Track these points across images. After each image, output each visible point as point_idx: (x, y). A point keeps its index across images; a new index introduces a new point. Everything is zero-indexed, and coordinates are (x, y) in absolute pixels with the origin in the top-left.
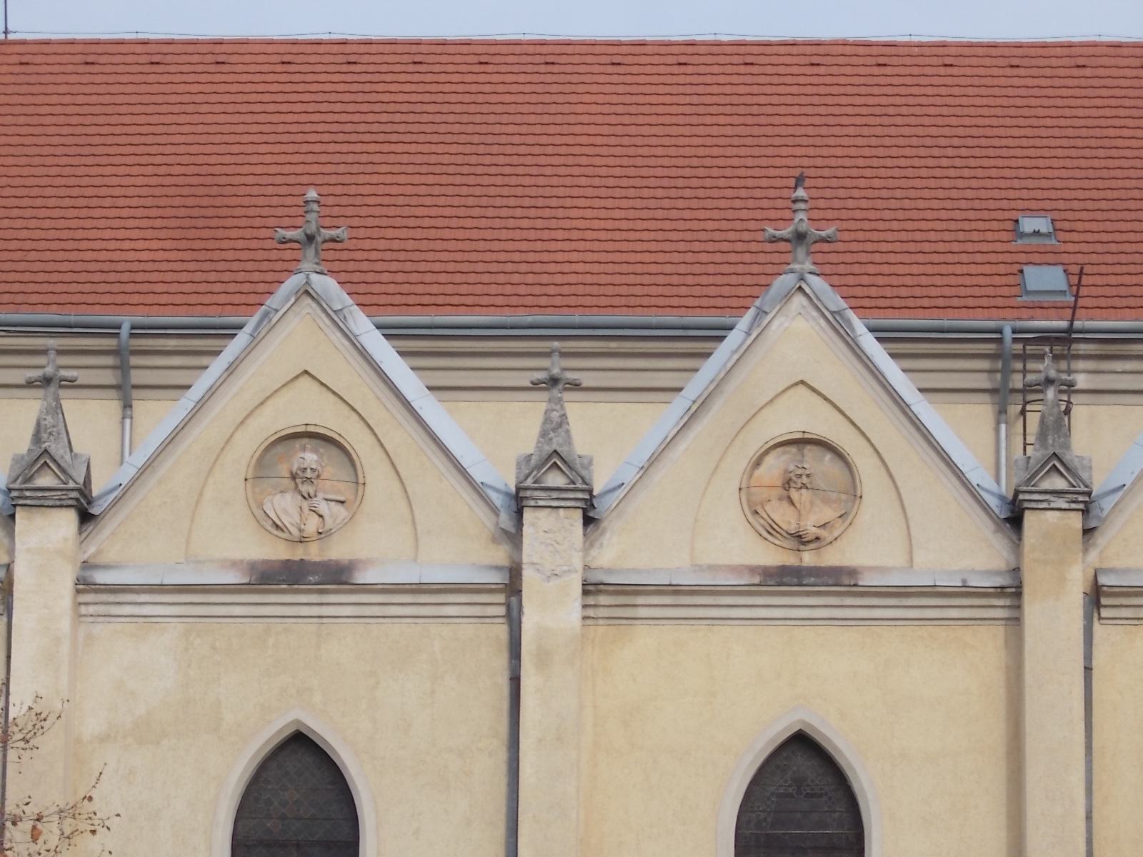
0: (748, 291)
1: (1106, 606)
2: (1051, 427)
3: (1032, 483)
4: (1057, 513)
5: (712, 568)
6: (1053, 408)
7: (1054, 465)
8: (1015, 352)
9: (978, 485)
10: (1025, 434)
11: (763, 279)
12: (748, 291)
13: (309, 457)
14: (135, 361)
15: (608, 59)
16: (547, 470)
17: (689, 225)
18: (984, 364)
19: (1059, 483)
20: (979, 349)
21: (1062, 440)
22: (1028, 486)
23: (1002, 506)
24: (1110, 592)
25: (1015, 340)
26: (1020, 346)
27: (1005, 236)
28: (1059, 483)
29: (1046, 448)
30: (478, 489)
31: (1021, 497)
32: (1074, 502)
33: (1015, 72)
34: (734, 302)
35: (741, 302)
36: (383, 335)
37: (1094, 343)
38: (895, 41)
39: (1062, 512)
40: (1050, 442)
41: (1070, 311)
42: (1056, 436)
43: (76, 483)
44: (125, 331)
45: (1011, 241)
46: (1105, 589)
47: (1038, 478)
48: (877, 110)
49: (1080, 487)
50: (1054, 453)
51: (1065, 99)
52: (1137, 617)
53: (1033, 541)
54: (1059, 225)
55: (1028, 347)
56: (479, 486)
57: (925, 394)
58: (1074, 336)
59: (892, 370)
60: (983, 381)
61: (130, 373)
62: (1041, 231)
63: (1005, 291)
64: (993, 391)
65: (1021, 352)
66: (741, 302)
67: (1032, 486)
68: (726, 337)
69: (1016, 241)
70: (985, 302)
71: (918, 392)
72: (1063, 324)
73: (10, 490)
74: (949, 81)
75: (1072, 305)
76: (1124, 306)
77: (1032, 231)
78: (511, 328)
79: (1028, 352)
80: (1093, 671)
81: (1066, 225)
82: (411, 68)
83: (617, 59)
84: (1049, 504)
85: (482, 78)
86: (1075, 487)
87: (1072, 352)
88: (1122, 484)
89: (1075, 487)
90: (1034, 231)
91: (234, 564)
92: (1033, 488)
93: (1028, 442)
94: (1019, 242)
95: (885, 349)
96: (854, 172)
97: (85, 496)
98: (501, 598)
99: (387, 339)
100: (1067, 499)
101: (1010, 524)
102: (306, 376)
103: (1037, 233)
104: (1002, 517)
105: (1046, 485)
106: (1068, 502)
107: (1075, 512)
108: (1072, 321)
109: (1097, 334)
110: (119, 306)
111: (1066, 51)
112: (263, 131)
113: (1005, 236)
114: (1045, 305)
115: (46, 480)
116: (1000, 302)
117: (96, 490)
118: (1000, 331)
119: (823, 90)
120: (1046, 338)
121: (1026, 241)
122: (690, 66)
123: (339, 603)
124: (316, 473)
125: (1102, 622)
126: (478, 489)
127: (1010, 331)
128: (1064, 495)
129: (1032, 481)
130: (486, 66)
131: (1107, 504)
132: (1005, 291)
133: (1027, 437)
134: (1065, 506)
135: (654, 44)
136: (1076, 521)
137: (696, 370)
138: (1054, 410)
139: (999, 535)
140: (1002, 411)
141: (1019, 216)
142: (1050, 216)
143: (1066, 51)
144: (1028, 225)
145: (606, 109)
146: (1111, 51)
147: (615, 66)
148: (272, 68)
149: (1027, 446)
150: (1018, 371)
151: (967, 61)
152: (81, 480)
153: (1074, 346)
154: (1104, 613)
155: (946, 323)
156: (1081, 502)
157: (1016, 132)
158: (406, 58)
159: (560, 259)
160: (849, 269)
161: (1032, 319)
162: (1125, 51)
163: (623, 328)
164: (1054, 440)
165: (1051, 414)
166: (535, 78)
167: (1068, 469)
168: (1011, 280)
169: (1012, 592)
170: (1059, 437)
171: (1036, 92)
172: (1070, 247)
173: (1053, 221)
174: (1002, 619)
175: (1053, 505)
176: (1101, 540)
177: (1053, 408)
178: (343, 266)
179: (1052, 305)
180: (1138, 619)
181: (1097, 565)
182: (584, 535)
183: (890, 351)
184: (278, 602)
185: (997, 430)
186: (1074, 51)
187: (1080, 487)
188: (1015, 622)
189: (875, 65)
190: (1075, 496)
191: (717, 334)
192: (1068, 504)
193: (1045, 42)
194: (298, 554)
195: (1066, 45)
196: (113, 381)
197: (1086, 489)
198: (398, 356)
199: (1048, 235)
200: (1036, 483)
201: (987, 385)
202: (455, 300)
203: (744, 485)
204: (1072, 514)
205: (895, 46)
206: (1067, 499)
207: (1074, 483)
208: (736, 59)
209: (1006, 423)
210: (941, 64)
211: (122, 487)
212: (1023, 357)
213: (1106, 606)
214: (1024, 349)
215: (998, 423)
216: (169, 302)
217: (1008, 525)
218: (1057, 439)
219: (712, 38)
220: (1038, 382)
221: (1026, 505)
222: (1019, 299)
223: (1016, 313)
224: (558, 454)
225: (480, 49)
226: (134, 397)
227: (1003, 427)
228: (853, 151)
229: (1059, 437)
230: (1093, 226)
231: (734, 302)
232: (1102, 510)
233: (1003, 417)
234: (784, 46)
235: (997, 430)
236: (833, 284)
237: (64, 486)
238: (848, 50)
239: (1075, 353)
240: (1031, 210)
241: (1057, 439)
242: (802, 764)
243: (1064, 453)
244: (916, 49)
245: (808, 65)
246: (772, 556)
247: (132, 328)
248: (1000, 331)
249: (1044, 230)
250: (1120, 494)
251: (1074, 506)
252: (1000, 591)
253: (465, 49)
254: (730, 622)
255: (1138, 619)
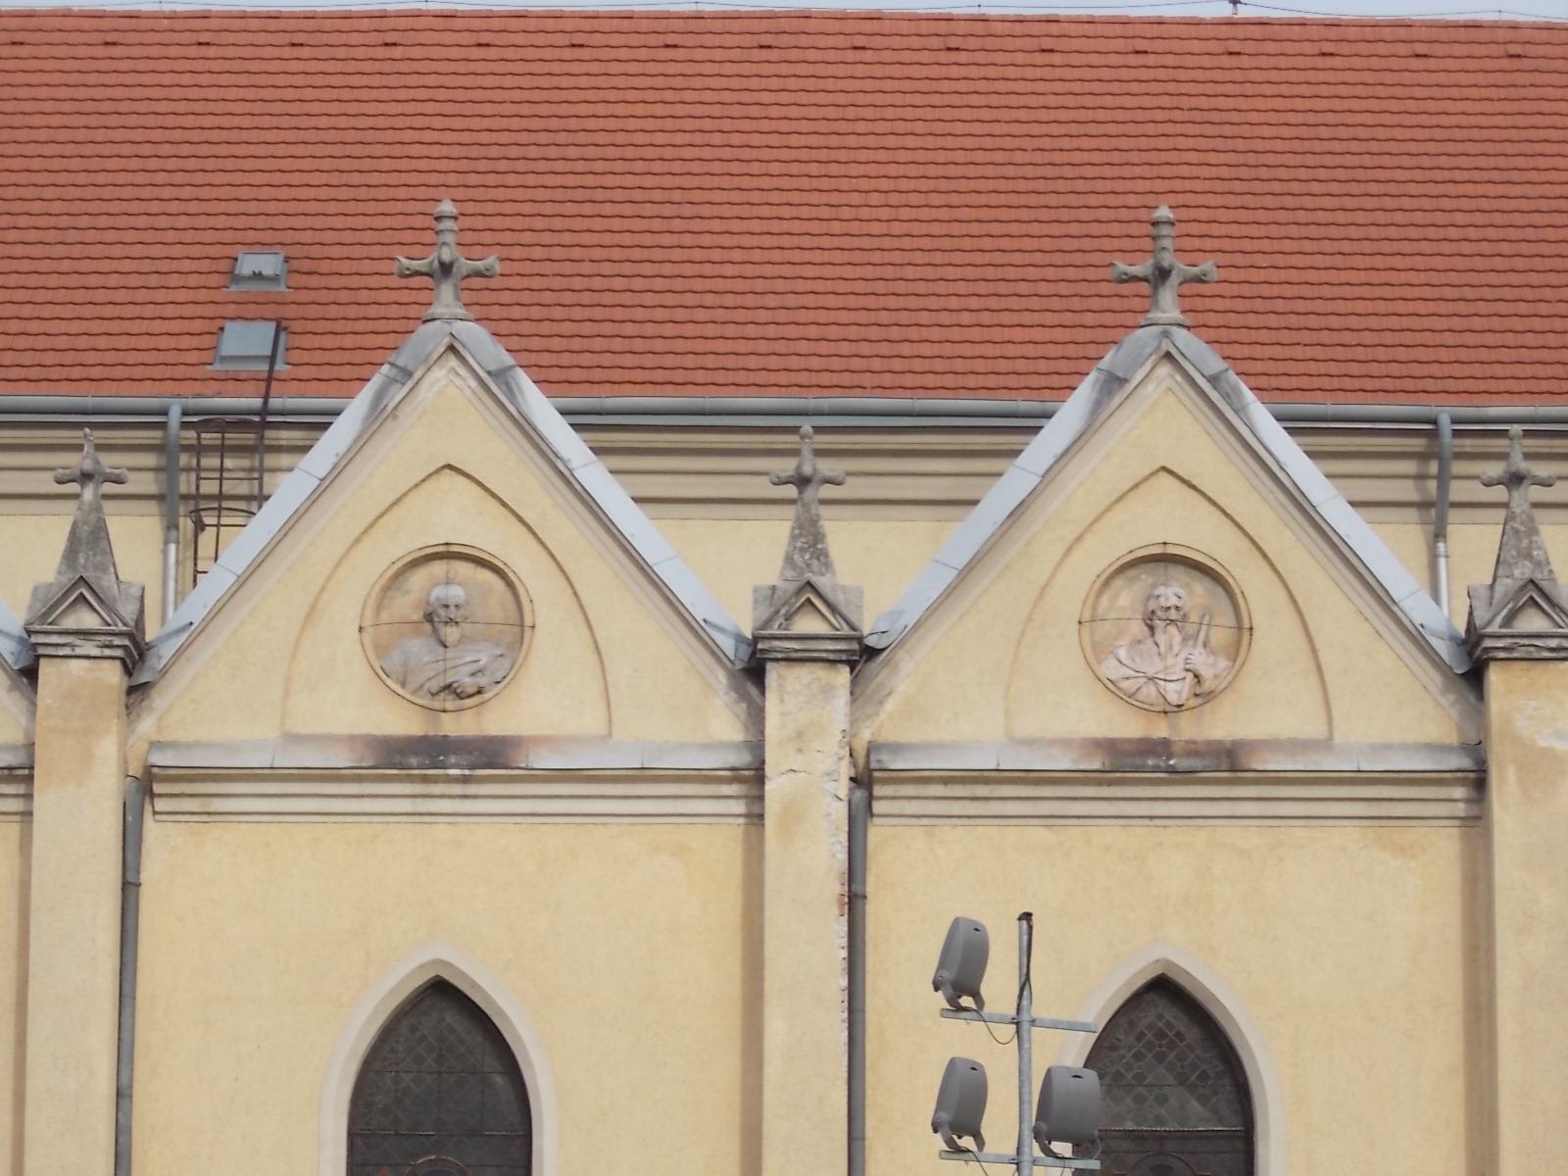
0: (1072, 366)
1: (161, 796)
2: (85, 540)
3: (50, 620)
4: (85, 663)
5: (1030, 743)
6: (90, 513)
7: (82, 594)
8: (183, 442)
9: (705, 621)
10: (196, 558)
11: (1091, 350)
12: (1072, 366)
13: (1175, 591)
14: (1458, 467)
15: (473, 38)
16: (68, 607)
17: (859, 272)
18: (1409, 467)
19: (88, 620)
20: (786, 443)
21: (99, 558)
22: (43, 624)
23: (20, 653)
24: (164, 775)
25: (185, 425)
26: (192, 434)
27: (214, 280)
28: (88, 620)
29: (75, 570)
30: (1417, 638)
31: (760, 646)
32: (107, 646)
33: (954, 57)
34: (1056, 381)
35: (356, 372)
36: (571, 425)
37: (300, 429)
38: (140, 11)
39: (93, 661)
40: (82, 561)
41: (263, 385)
42: (91, 553)
43: (125, 624)
44: (175, 417)
45: (222, 287)
46: (155, 770)
47: (58, 612)
48: (87, 107)
49: (116, 626)
50: (82, 577)
51: (1117, 97)
52: (206, 810)
53: (49, 701)
54: (295, 265)
55: (203, 435)
56: (700, 625)
57: (1360, 509)
58: (270, 419)
59: (593, 474)
60: (1407, 491)
61: (1448, 485)
62: (264, 273)
63: (192, 357)
64: (1423, 505)
65: (194, 442)
66: (356, 372)
67: (50, 624)
68: (1041, 427)
69: (227, 287)
70: (157, 372)
71: (632, 502)
72: (256, 402)
73: (29, 633)
74: (1048, 73)
75: (265, 375)
76: (1316, 387)
77: (251, 273)
78: (1023, 417)
79: (203, 442)
80: (142, 888)
81: (307, 265)
82: (288, 52)
83: (484, 38)
84: (73, 650)
85: (575, 68)
86: (109, 625)
87: (267, 442)
88: (189, 621)
89: (109, 625)
90: (254, 273)
91: (351, 739)
92: (49, 627)
93: (199, 569)
94: (233, 288)
95: (584, 441)
96: (579, 194)
97: (136, 643)
98: (1459, 792)
99: (576, 430)
100: (98, 643)
101: (27, 678)
102: (447, 471)
103: (258, 276)
104: (16, 668)
105: (70, 622)
106: (98, 647)
107: (110, 661)
108: (266, 398)
109: (72, 416)
110: (54, 383)
111: (1118, 30)
112: (210, 140)
113: (214, 280)
114: (243, 376)
115: (808, 624)
116: (180, 372)
117: (151, 633)
118: (165, 413)
119: (888, 85)
120: (239, 421)
121: (244, 287)
122: (494, 49)
123: (491, 797)
124: (1182, 613)
125: (158, 817)
126: (1417, 638)
127: (1449, 421)
128: (93, 637)
129: (50, 616)
130: (768, 51)
131: (167, 651)
132: (192, 357)
133: (199, 562)
134: (96, 652)
135: (573, 16)
136: (112, 675)
137: (1000, 475)
138: (92, 516)
139: (1452, 697)
140: (171, 525)
141: (238, 250)
142: (283, 253)
143: (1118, 30)
144: (248, 264)
145: (449, 108)
146: (441, 23)
147: (1045, 54)
148: (277, 52)
149: (199, 575)
150: (1432, 477)
151: (232, 38)
152: (130, 618)
153: (270, 434)
154: (161, 805)
155: (90, 402)
156: (118, 646)
157: (1317, 146)
158: (936, 42)
159: (802, 320)
160: (863, 332)
161: (219, 395)
162: (457, 24)
163: (70, 414)
164: (87, 559)
165: (86, 523)
166: (839, 70)
167: (100, 600)
168: (206, 342)
169: (25, 775)
170: (95, 555)
171: (1153, 87)
172: (304, 296)
173: (287, 259)
174: (16, 814)
175: (78, 651)
176: (159, 701)
177: (90, 513)
178: (514, 327)
179: (252, 377)
180: (209, 813)
181: (154, 737)
182: (852, 694)
183: (1308, 449)
184: (396, 796)
185: (165, 552)
186: (1414, 33)
187: (116, 626)
188: (1476, 821)
189: (850, 48)
190: (109, 638)
191: (1030, 425)
192: (99, 649)
193: (350, 11)
194: (1160, 730)
195: (377, 15)
196: (153, 489)
197: (125, 628)
198: (1307, 457)
199: (275, 279)
200: (54, 620)
201: (1414, 497)
202: (617, 375)
203: (367, 623)
204: (106, 664)
205: (138, 17)
206: (98, 643)
207: (836, 624)
208: (653, 40)
209: (178, 543)
210: (1037, 48)
211: (193, 627)
212: (198, 450)
213: (161, 796)
214: (199, 438)
215: (166, 543)
216: (43, 377)
217: (25, 680)
218: (91, 558)
219: (975, 11)
220: (71, 477)
221: (41, 651)
222: (209, 367)
223: (198, 386)
224: (85, 580)
225: (292, 24)
226: (1450, 520)
227: (172, 547)
228: (872, 170)
229: (95, 555)
230: (1413, 277)
231: (1056, 381)
232: (160, 658)
233: (173, 534)
234: (516, 19)
235: (165, 552)
236: (511, 349)
237: (108, 628)
238: (69, 23)
239: (275, 443)
240: (262, 244)
241: (91, 558)
242: (1166, 1013)
243: (99, 577)
244: (166, 21)
245: (661, 47)
246: (400, 721)
247: (185, 413)
248: (1434, 422)
249: (267, 271)
250: (185, 635)
251: (107, 652)
252: (735, 775)
253: (273, 25)
254: (1330, 822)
255: (209, 813)
